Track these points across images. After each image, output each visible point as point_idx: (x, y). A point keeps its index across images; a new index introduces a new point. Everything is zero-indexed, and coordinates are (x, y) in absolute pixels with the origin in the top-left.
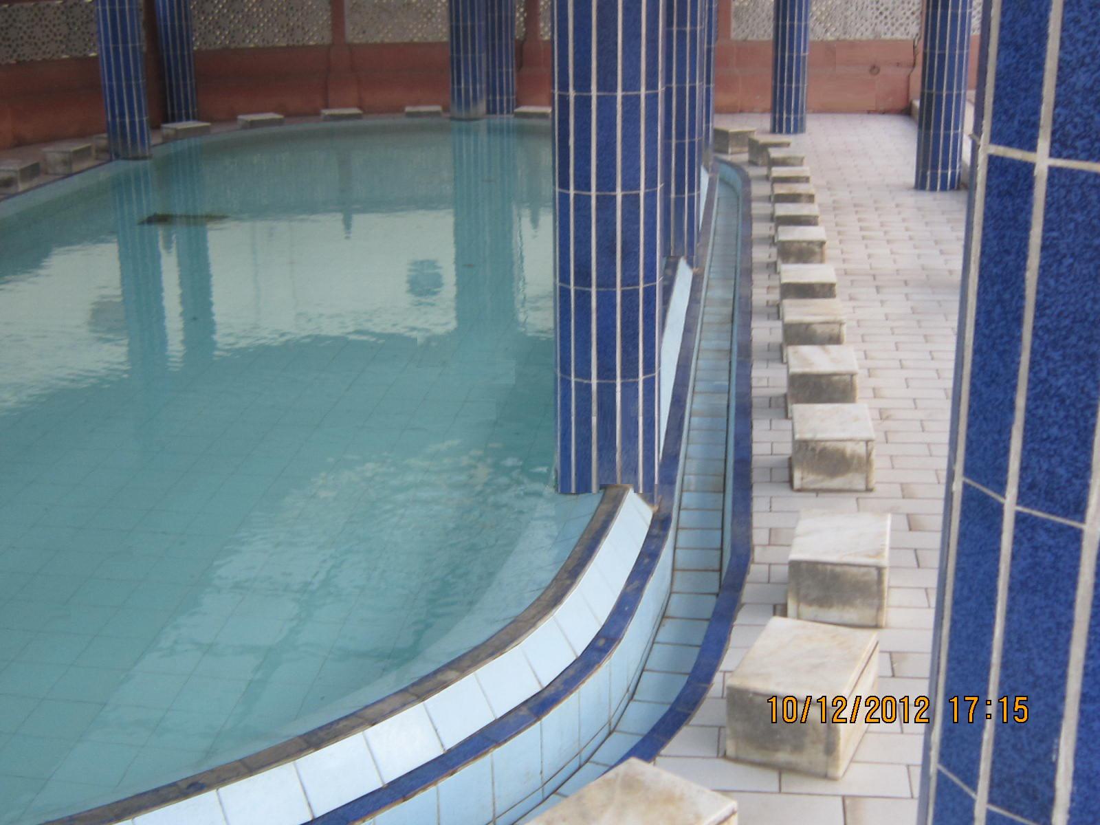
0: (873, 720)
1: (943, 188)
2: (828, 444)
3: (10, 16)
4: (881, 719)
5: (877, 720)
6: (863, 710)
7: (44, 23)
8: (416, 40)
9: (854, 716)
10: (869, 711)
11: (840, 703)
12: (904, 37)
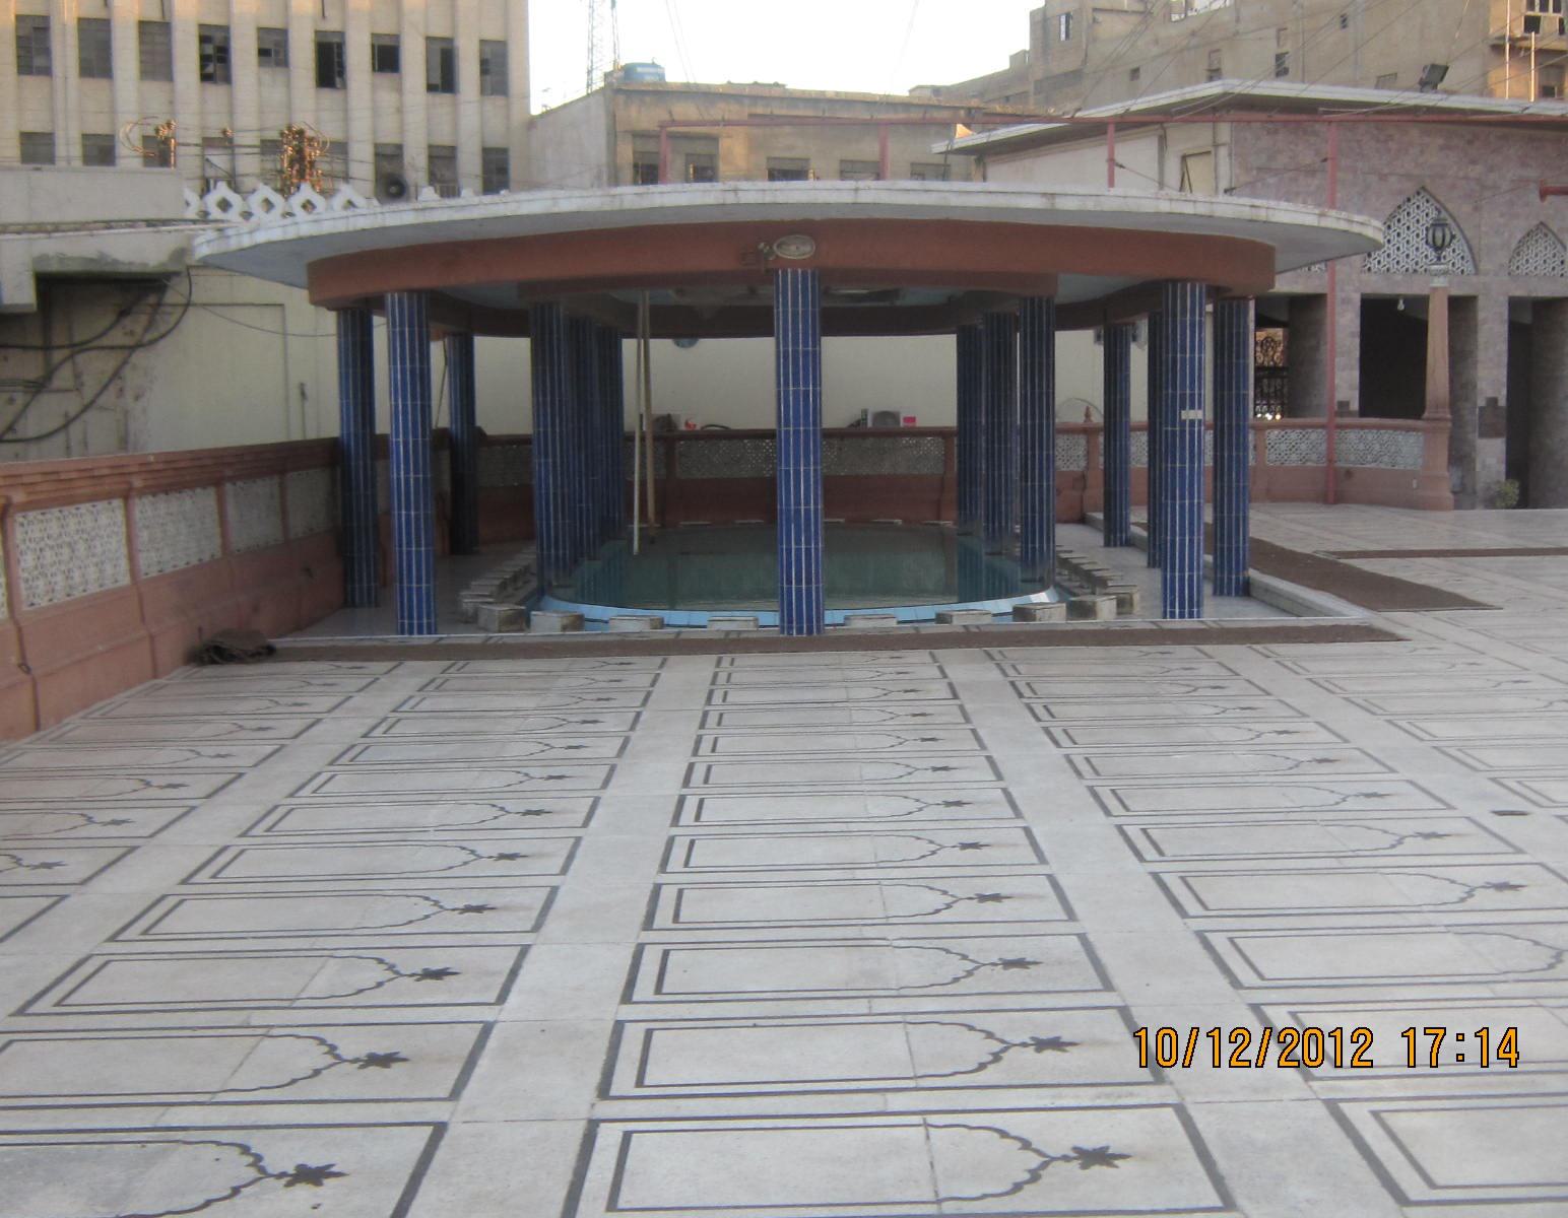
0: (1240, 1064)
1: (1121, 545)
5: (1296, 1064)
9: (1261, 1058)
11: (1240, 1038)
12: (1076, 469)
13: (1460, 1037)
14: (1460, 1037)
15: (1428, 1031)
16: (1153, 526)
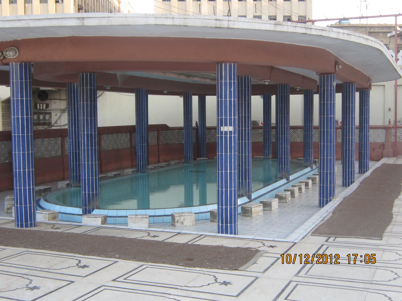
0: (319, 263)
2: (280, 195)
3: (166, 133)
4: (322, 262)
5: (321, 263)
6: (316, 259)
7: (173, 135)
8: (260, 141)
10: (318, 260)
11: (307, 257)
13: (361, 256)
14: (361, 256)
15: (353, 255)
16: (177, 130)
